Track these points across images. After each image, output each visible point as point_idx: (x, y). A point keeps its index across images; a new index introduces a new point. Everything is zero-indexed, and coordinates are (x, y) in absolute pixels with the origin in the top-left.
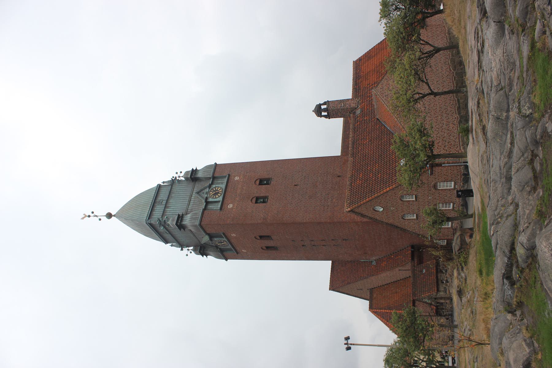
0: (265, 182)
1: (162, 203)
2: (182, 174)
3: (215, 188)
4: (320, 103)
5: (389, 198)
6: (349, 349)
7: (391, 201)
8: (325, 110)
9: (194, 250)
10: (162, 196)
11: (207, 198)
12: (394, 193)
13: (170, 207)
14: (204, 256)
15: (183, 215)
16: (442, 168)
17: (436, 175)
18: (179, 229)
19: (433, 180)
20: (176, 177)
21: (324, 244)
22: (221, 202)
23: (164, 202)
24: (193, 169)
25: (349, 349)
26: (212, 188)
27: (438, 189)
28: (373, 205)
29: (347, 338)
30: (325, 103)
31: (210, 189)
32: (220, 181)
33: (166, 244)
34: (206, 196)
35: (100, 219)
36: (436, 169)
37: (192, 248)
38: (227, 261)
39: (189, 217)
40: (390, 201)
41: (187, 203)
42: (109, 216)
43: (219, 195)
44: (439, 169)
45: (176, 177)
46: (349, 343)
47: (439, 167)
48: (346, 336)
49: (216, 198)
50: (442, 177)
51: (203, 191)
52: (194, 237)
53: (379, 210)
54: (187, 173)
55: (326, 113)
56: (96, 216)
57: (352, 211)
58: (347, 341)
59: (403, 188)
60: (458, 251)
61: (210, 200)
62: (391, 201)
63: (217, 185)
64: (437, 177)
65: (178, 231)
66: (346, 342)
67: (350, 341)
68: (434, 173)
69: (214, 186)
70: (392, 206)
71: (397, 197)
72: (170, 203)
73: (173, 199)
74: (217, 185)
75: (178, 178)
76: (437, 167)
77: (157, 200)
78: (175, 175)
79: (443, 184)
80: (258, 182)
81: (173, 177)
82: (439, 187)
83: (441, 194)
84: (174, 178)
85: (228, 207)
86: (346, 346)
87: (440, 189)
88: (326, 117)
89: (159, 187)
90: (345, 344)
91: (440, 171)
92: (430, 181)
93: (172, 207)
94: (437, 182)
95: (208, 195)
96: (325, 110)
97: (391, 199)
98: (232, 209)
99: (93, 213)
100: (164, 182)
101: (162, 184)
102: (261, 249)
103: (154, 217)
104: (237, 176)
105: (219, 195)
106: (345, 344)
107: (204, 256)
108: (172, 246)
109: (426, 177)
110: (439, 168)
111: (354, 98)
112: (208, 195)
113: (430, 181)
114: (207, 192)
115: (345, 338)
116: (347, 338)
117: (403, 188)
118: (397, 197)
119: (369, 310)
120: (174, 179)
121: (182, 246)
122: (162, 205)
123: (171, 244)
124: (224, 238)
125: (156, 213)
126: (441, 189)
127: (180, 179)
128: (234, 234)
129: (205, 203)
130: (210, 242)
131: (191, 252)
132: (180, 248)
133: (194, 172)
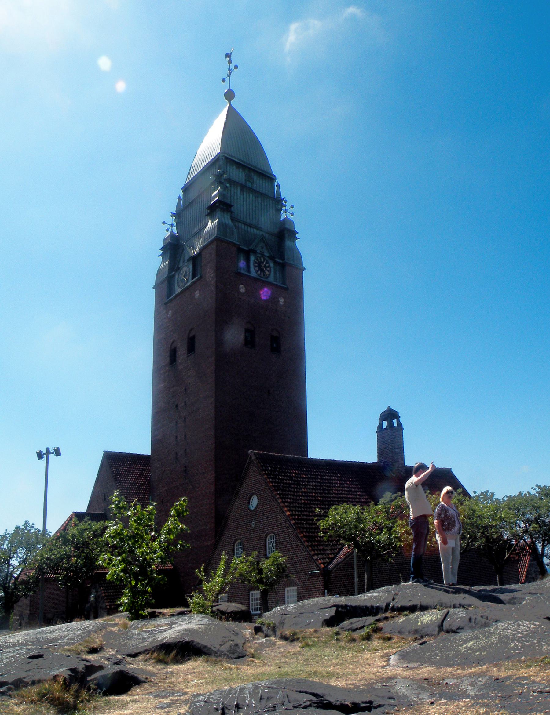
0: (275, 345)
1: (248, 182)
2: (290, 217)
3: (269, 267)
4: (400, 417)
5: (272, 517)
6: (40, 455)
7: (266, 520)
8: (391, 425)
9: (172, 235)
10: (258, 181)
11: (254, 252)
12: (281, 523)
13: (242, 194)
14: (162, 251)
15: (232, 212)
16: (322, 590)
17: (311, 582)
18: (207, 207)
19: (300, 579)
20: (285, 206)
21: (179, 438)
22: (249, 274)
23: (249, 185)
24: (298, 233)
25: (40, 455)
26: (270, 261)
27: (284, 589)
28: (260, 494)
29: (57, 452)
30: (400, 424)
31: (267, 258)
32: (278, 275)
33: (182, 189)
34: (259, 251)
35: (236, 67)
36: (319, 581)
37: (175, 230)
38: (153, 288)
39: (227, 222)
40: (267, 518)
41: (248, 221)
42: (230, 95)
43: (259, 272)
44: (319, 585)
45: (285, 206)
46: (50, 455)
47: (324, 585)
48: (61, 450)
49: (255, 266)
50: (305, 591)
51: (265, 248)
52: (193, 233)
53: (251, 505)
54: (292, 223)
55: (393, 421)
56: (230, 73)
57: (250, 463)
58: (53, 453)
59: (288, 536)
60: (218, 610)
61: (252, 258)
62: (266, 520)
63: (272, 270)
64: (306, 585)
65: (205, 206)
66: (51, 450)
67: (52, 457)
68: (314, 580)
69: (272, 265)
70: (257, 522)
71: (274, 529)
72: (248, 195)
73: (254, 199)
74: (272, 270)
75: (284, 208)
76: (323, 583)
77: (252, 174)
78: (288, 205)
79: (293, 595)
80: (275, 334)
81: (286, 202)
82: (288, 590)
83: (277, 594)
84: (285, 203)
85: (241, 286)
86: (45, 451)
87: (284, 591)
88: (381, 425)
89: (270, 178)
90: (48, 449)
91: (316, 588)
92: (299, 575)
93: (242, 197)
94: (298, 586)
95: (258, 255)
96: (391, 425)
97: (270, 520)
98: (239, 292)
99: (236, 67)
100: (278, 186)
101: (276, 183)
102: (172, 341)
103: (228, 168)
104: (285, 301)
105: (259, 272)
106: (48, 449)
107: (162, 251)
108: (179, 198)
109: (307, 567)
110: (322, 585)
111: (405, 468)
112: (258, 255)
113: (299, 575)
114: (263, 253)
115: (58, 448)
116: (57, 452)
117: (288, 536)
118: (274, 529)
119: (74, 512)
120: (283, 202)
121: (178, 215)
122: (246, 181)
123: (182, 197)
124: (192, 279)
125: (234, 170)
126: (284, 594)
127: (282, 212)
128: (198, 295)
129: (247, 249)
130: (187, 258)
131: (167, 230)
132: (175, 213)
133: (293, 234)
